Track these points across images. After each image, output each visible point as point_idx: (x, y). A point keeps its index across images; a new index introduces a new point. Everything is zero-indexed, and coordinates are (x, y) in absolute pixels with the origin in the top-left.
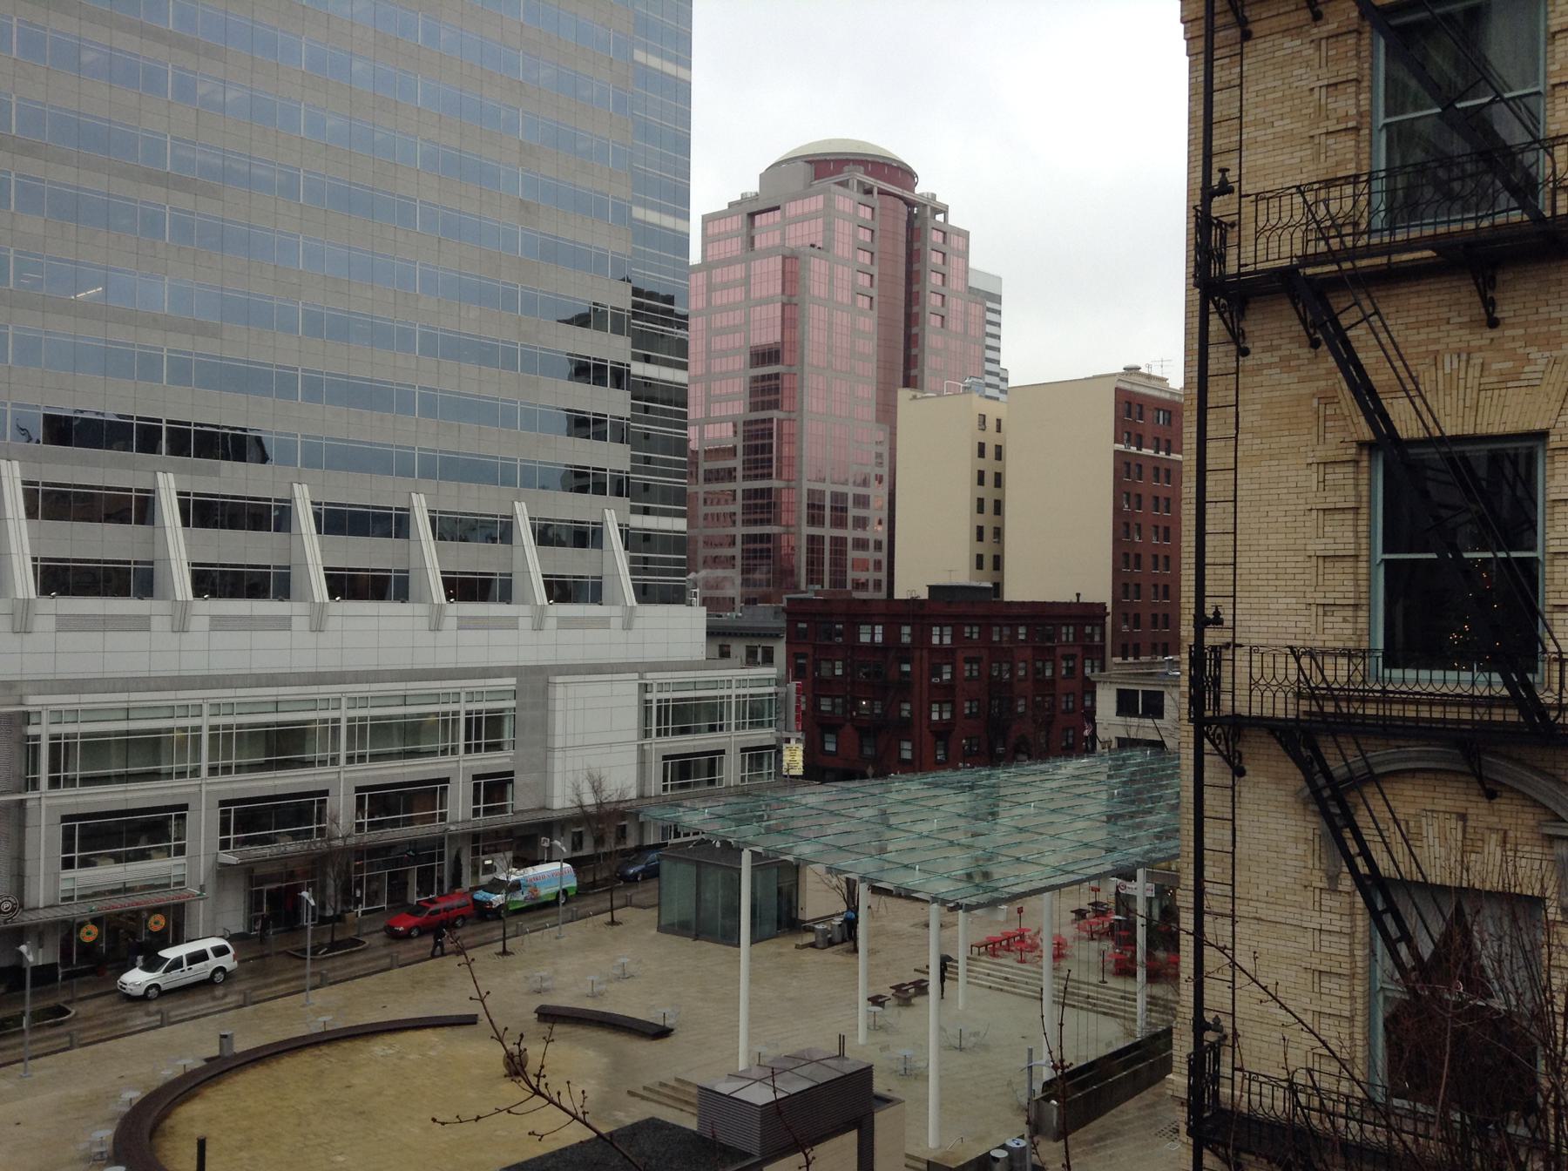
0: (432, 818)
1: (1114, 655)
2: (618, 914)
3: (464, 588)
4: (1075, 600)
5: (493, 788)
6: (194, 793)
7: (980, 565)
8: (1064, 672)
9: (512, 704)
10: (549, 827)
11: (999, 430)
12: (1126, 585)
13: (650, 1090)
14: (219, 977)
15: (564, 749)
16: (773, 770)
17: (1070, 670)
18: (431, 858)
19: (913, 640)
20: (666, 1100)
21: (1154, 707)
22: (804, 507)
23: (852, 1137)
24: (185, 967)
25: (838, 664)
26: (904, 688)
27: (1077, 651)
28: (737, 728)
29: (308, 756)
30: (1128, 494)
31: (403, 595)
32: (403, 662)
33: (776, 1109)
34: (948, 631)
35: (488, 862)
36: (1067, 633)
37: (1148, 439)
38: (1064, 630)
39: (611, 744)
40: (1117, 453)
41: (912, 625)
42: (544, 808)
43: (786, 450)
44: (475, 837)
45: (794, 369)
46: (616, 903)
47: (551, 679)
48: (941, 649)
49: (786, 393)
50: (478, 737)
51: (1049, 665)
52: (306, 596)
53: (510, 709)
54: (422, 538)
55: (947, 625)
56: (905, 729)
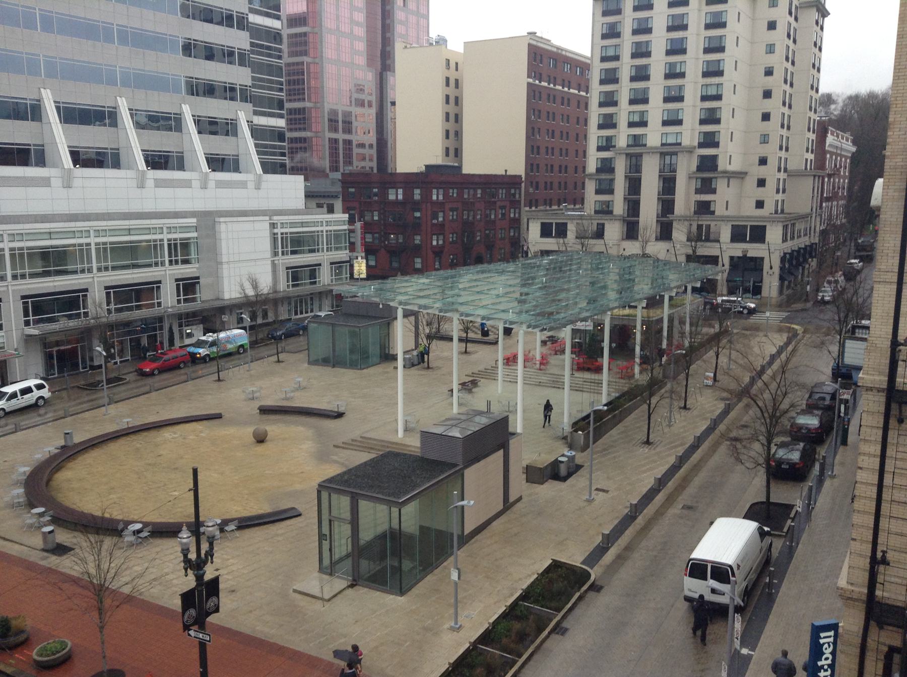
0: (152, 305)
1: (525, 206)
2: (282, 356)
3: (156, 161)
4: (504, 173)
5: (188, 287)
6: (4, 291)
7: (447, 155)
8: (500, 216)
9: (195, 235)
10: (222, 310)
11: (457, 70)
12: (532, 165)
13: (356, 441)
14: (41, 402)
15: (228, 263)
16: (348, 275)
17: (503, 215)
18: (155, 329)
19: (421, 197)
20: (355, 448)
21: (562, 231)
22: (326, 120)
23: (501, 452)
24: (19, 397)
25: (376, 213)
26: (417, 227)
27: (507, 204)
28: (327, 251)
29: (70, 267)
30: (534, 110)
31: (116, 165)
32: (123, 208)
33: (467, 439)
34: (441, 191)
35: (188, 331)
36: (502, 193)
37: (544, 76)
38: (500, 191)
39: (255, 260)
40: (529, 84)
41: (421, 188)
42: (218, 299)
43: (313, 83)
44: (180, 316)
45: (316, 30)
46: (280, 350)
47: (217, 219)
48: (437, 203)
49: (311, 45)
50: (176, 256)
51: (493, 212)
52: (57, 164)
53: (194, 238)
54: (127, 127)
55: (441, 188)
56: (417, 250)
